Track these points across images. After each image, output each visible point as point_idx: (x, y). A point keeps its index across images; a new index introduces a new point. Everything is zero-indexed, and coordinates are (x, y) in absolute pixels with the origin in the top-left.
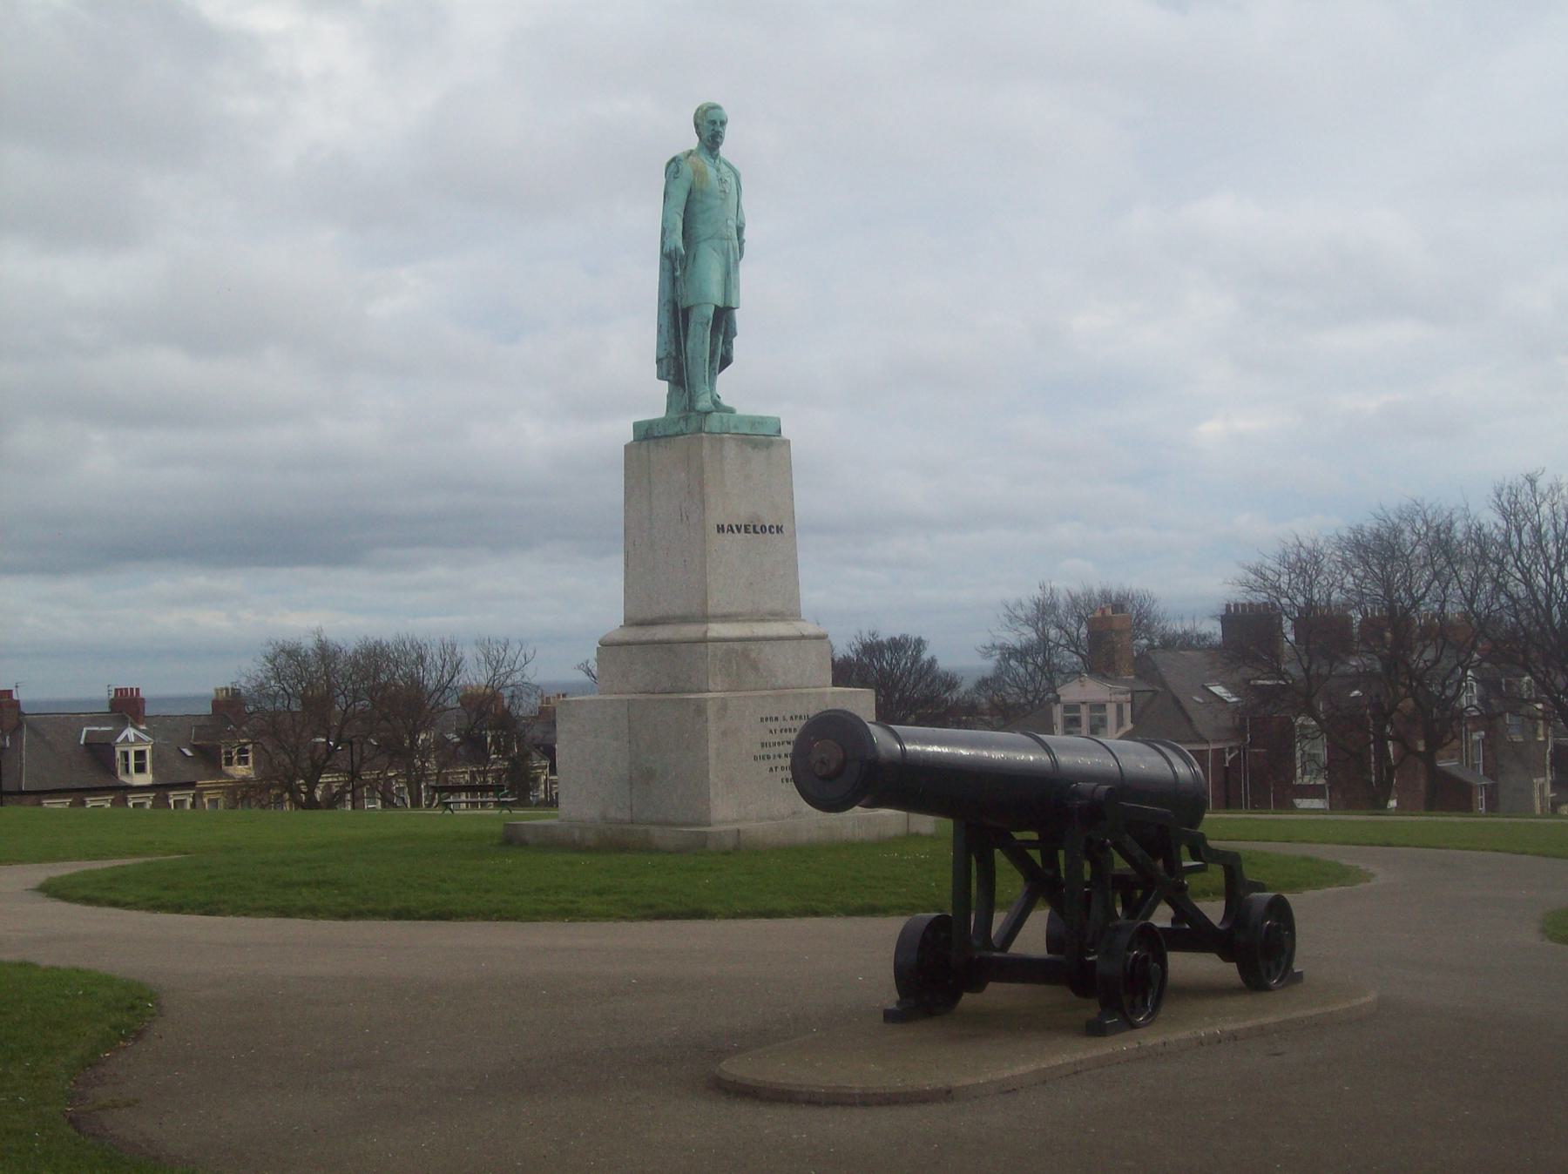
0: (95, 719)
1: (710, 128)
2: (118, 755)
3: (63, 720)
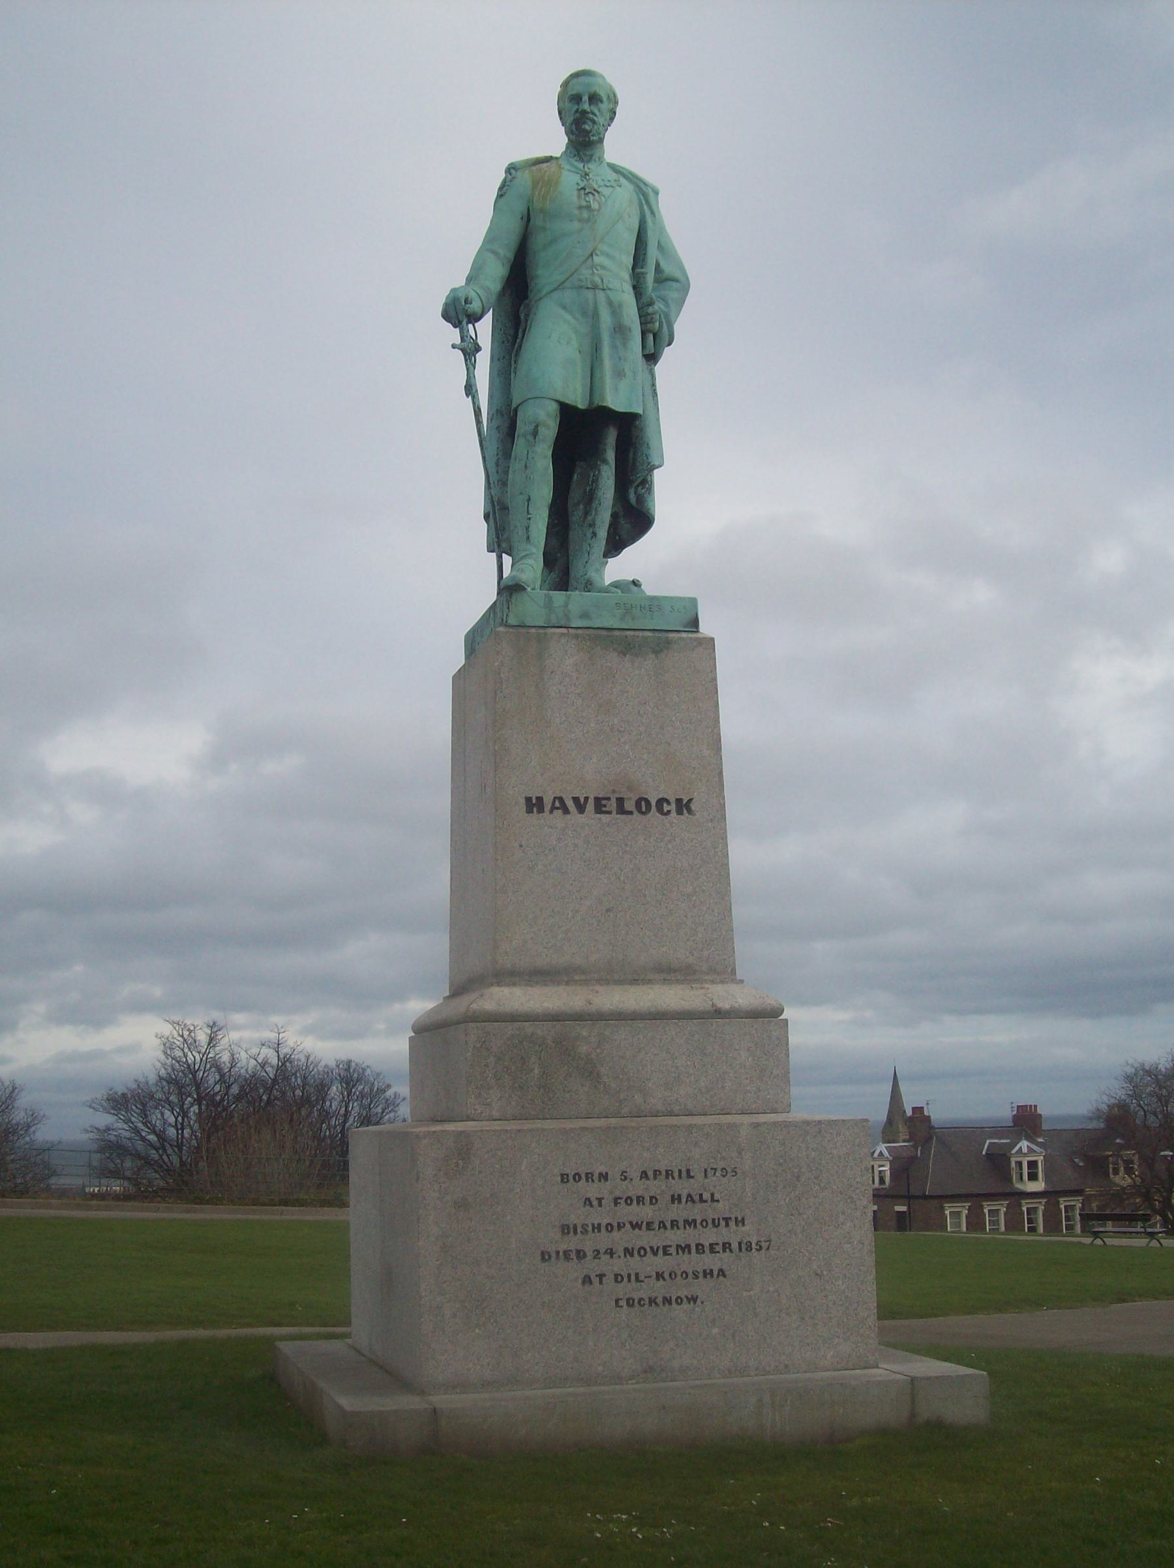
0: (997, 1131)
1: (584, 111)
2: (1013, 1165)
3: (971, 1133)
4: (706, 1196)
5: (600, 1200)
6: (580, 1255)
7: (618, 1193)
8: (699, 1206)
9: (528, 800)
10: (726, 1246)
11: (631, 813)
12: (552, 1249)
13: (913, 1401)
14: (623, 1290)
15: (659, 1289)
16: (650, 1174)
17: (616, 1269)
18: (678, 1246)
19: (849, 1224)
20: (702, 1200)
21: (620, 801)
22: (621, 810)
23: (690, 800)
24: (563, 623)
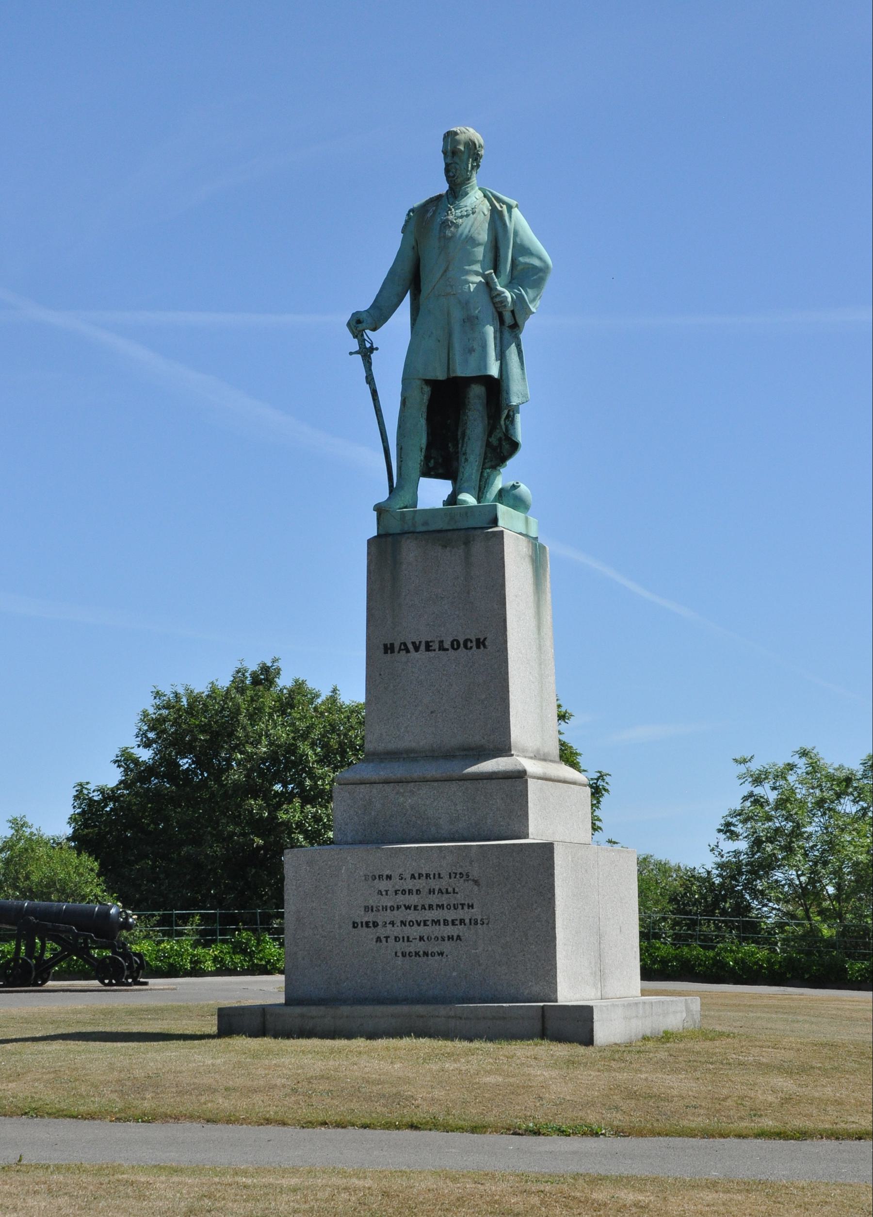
4: (450, 890)
5: (387, 891)
6: (375, 924)
7: (397, 887)
8: (445, 896)
9: (385, 646)
10: (462, 921)
11: (447, 650)
12: (358, 920)
13: (543, 1022)
14: (400, 946)
15: (421, 947)
16: (416, 875)
17: (396, 934)
18: (433, 921)
19: (539, 909)
20: (447, 892)
21: (441, 642)
22: (442, 648)
23: (485, 639)
24: (412, 529)
